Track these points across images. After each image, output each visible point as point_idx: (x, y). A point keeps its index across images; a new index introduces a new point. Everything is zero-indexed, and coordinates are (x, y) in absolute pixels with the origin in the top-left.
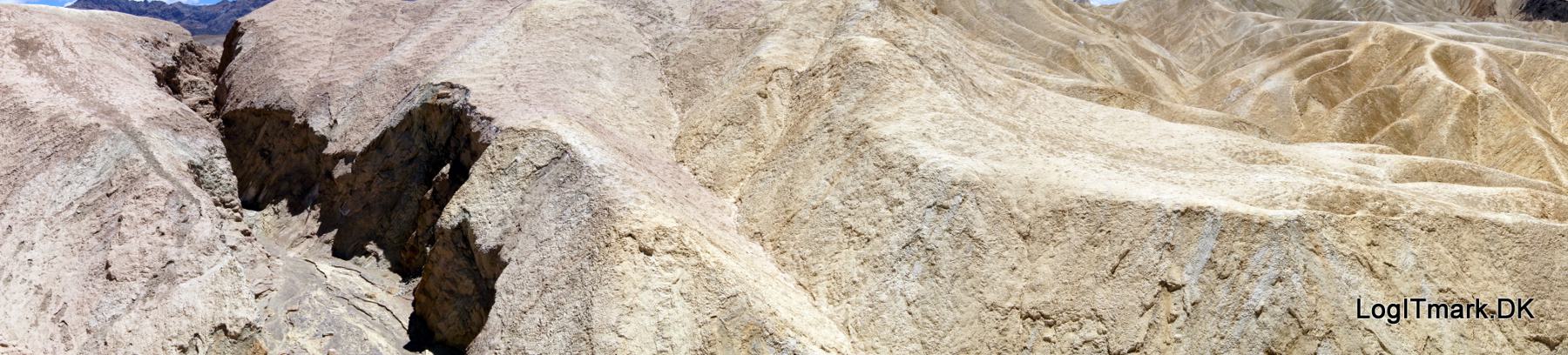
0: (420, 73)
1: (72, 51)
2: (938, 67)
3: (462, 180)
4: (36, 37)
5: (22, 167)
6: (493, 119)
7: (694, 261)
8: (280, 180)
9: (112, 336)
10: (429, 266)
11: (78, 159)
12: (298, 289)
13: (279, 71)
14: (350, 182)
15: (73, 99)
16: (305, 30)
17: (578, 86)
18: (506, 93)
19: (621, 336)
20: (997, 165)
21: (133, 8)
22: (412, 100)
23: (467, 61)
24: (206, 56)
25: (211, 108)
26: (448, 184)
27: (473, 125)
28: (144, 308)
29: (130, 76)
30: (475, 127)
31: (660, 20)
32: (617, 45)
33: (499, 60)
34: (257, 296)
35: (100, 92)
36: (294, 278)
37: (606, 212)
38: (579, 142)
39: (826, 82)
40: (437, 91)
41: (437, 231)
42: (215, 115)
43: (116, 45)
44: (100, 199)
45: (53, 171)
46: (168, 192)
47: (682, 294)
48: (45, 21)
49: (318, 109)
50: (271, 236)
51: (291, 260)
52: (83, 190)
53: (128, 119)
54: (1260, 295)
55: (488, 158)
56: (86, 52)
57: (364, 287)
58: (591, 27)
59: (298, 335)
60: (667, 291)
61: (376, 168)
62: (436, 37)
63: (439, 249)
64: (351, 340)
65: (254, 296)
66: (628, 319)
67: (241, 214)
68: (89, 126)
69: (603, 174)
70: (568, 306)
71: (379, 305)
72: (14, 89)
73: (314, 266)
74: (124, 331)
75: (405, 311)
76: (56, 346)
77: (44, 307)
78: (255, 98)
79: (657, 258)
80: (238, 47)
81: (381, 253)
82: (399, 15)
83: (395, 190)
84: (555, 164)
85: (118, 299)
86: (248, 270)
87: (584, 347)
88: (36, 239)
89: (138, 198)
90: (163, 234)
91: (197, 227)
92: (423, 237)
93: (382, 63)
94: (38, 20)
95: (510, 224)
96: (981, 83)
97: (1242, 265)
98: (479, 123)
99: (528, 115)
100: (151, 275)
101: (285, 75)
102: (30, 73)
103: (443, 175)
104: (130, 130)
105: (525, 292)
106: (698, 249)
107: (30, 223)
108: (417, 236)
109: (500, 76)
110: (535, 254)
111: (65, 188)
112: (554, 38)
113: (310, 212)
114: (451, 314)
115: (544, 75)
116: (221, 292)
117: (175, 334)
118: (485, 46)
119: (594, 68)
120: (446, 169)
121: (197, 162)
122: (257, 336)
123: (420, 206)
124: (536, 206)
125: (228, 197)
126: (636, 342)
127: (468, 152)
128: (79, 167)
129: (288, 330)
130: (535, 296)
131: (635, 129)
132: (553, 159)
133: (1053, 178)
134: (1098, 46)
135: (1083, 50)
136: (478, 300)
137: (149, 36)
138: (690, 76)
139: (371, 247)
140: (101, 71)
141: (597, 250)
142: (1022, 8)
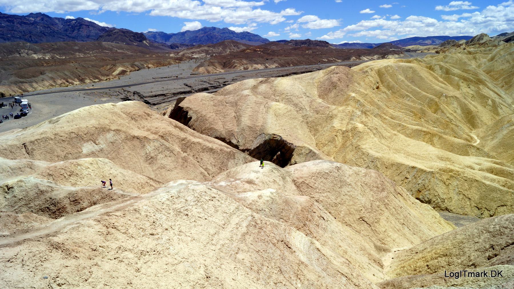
2: (375, 131)
20: (383, 155)
39: (350, 134)
54: (420, 182)
96: (384, 135)
97: (419, 177)
133: (393, 158)
134: (452, 97)
135: (444, 98)
138: (315, 128)
142: (418, 78)
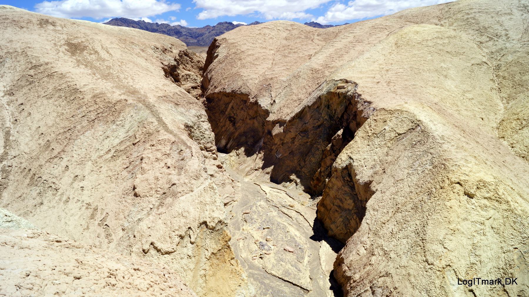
0: (327, 73)
1: (108, 52)
3: (350, 139)
4: (82, 42)
5: (75, 127)
6: (372, 102)
7: (505, 206)
8: (240, 135)
9: (138, 232)
10: (327, 190)
11: (113, 122)
12: (250, 200)
13: (241, 70)
14: (282, 138)
15: (109, 84)
16: (258, 45)
17: (431, 83)
18: (381, 86)
19: (445, 248)
21: (149, 27)
22: (322, 90)
23: (357, 66)
24: (196, 59)
25: (199, 91)
26: (341, 142)
27: (359, 106)
28: (158, 213)
29: (147, 70)
30: (360, 107)
31: (496, 39)
32: (461, 57)
33: (378, 66)
34: (225, 204)
35: (127, 79)
36: (247, 194)
37: (443, 166)
38: (428, 120)
40: (337, 84)
41: (333, 169)
42: (202, 96)
43: (137, 50)
44: (128, 146)
45: (97, 129)
46: (172, 142)
47: (492, 228)
48: (88, 32)
49: (264, 93)
50: (234, 168)
51: (246, 183)
52: (117, 141)
53: (146, 97)
55: (367, 127)
56: (117, 54)
57: (288, 201)
58: (443, 45)
59: (249, 228)
60: (481, 223)
61: (298, 130)
62: (338, 51)
63: (333, 180)
64: (279, 231)
65: (223, 204)
66: (451, 238)
67: (217, 155)
68: (120, 101)
69: (443, 141)
70: (411, 223)
71: (296, 212)
72: (68, 75)
73: (259, 187)
74: (146, 227)
75: (312, 216)
76: (102, 241)
77: (92, 217)
78: (226, 86)
79: (477, 200)
80: (216, 54)
81: (298, 181)
82: (316, 37)
83: (308, 144)
84: (410, 132)
85: (142, 208)
86: (221, 189)
87: (419, 251)
88: (86, 173)
89: (153, 146)
90: (169, 167)
91: (190, 163)
92: (324, 173)
93: (304, 67)
94: (83, 31)
95: (378, 168)
98: (362, 105)
99: (395, 101)
100: (162, 192)
101: (244, 72)
102: (78, 66)
103: (338, 135)
104: (147, 104)
105: (385, 211)
106: (509, 199)
107: (81, 163)
108: (320, 172)
109: (378, 76)
110: (392, 188)
111: (105, 140)
112: (417, 52)
113: (257, 155)
114: (339, 220)
115: (408, 76)
116: (204, 202)
117: (177, 228)
118: (370, 57)
119: (443, 72)
120: (340, 132)
121: (190, 124)
122: (225, 228)
123: (323, 154)
124: (396, 158)
125: (209, 145)
126: (456, 254)
127: (354, 122)
128: (114, 127)
129: (243, 225)
130: (390, 214)
131: (469, 114)
132: (410, 129)
136: (355, 213)
137: (159, 46)
139: (293, 177)
140: (127, 66)
141: (434, 190)
